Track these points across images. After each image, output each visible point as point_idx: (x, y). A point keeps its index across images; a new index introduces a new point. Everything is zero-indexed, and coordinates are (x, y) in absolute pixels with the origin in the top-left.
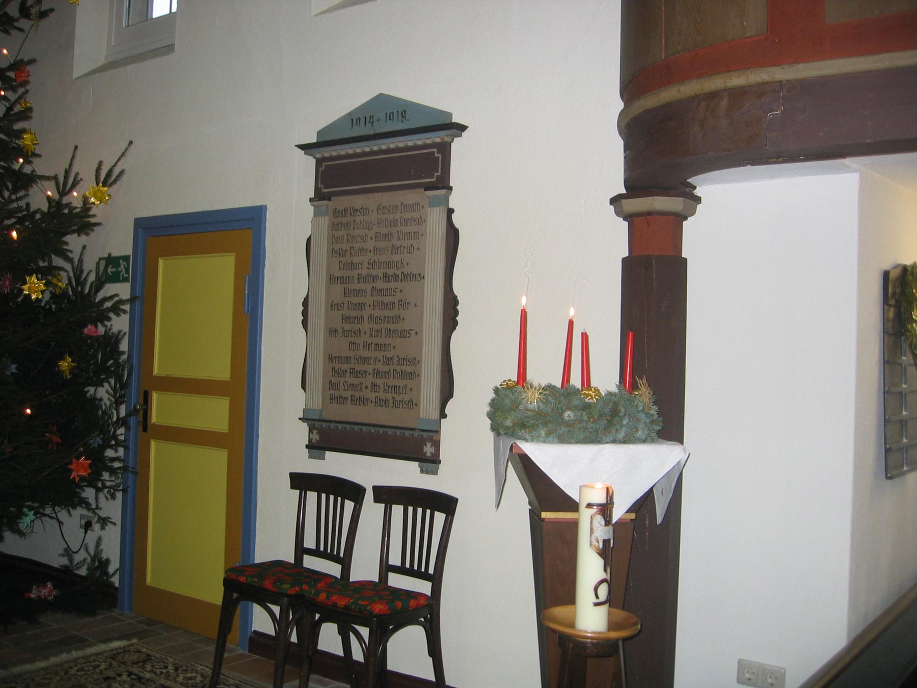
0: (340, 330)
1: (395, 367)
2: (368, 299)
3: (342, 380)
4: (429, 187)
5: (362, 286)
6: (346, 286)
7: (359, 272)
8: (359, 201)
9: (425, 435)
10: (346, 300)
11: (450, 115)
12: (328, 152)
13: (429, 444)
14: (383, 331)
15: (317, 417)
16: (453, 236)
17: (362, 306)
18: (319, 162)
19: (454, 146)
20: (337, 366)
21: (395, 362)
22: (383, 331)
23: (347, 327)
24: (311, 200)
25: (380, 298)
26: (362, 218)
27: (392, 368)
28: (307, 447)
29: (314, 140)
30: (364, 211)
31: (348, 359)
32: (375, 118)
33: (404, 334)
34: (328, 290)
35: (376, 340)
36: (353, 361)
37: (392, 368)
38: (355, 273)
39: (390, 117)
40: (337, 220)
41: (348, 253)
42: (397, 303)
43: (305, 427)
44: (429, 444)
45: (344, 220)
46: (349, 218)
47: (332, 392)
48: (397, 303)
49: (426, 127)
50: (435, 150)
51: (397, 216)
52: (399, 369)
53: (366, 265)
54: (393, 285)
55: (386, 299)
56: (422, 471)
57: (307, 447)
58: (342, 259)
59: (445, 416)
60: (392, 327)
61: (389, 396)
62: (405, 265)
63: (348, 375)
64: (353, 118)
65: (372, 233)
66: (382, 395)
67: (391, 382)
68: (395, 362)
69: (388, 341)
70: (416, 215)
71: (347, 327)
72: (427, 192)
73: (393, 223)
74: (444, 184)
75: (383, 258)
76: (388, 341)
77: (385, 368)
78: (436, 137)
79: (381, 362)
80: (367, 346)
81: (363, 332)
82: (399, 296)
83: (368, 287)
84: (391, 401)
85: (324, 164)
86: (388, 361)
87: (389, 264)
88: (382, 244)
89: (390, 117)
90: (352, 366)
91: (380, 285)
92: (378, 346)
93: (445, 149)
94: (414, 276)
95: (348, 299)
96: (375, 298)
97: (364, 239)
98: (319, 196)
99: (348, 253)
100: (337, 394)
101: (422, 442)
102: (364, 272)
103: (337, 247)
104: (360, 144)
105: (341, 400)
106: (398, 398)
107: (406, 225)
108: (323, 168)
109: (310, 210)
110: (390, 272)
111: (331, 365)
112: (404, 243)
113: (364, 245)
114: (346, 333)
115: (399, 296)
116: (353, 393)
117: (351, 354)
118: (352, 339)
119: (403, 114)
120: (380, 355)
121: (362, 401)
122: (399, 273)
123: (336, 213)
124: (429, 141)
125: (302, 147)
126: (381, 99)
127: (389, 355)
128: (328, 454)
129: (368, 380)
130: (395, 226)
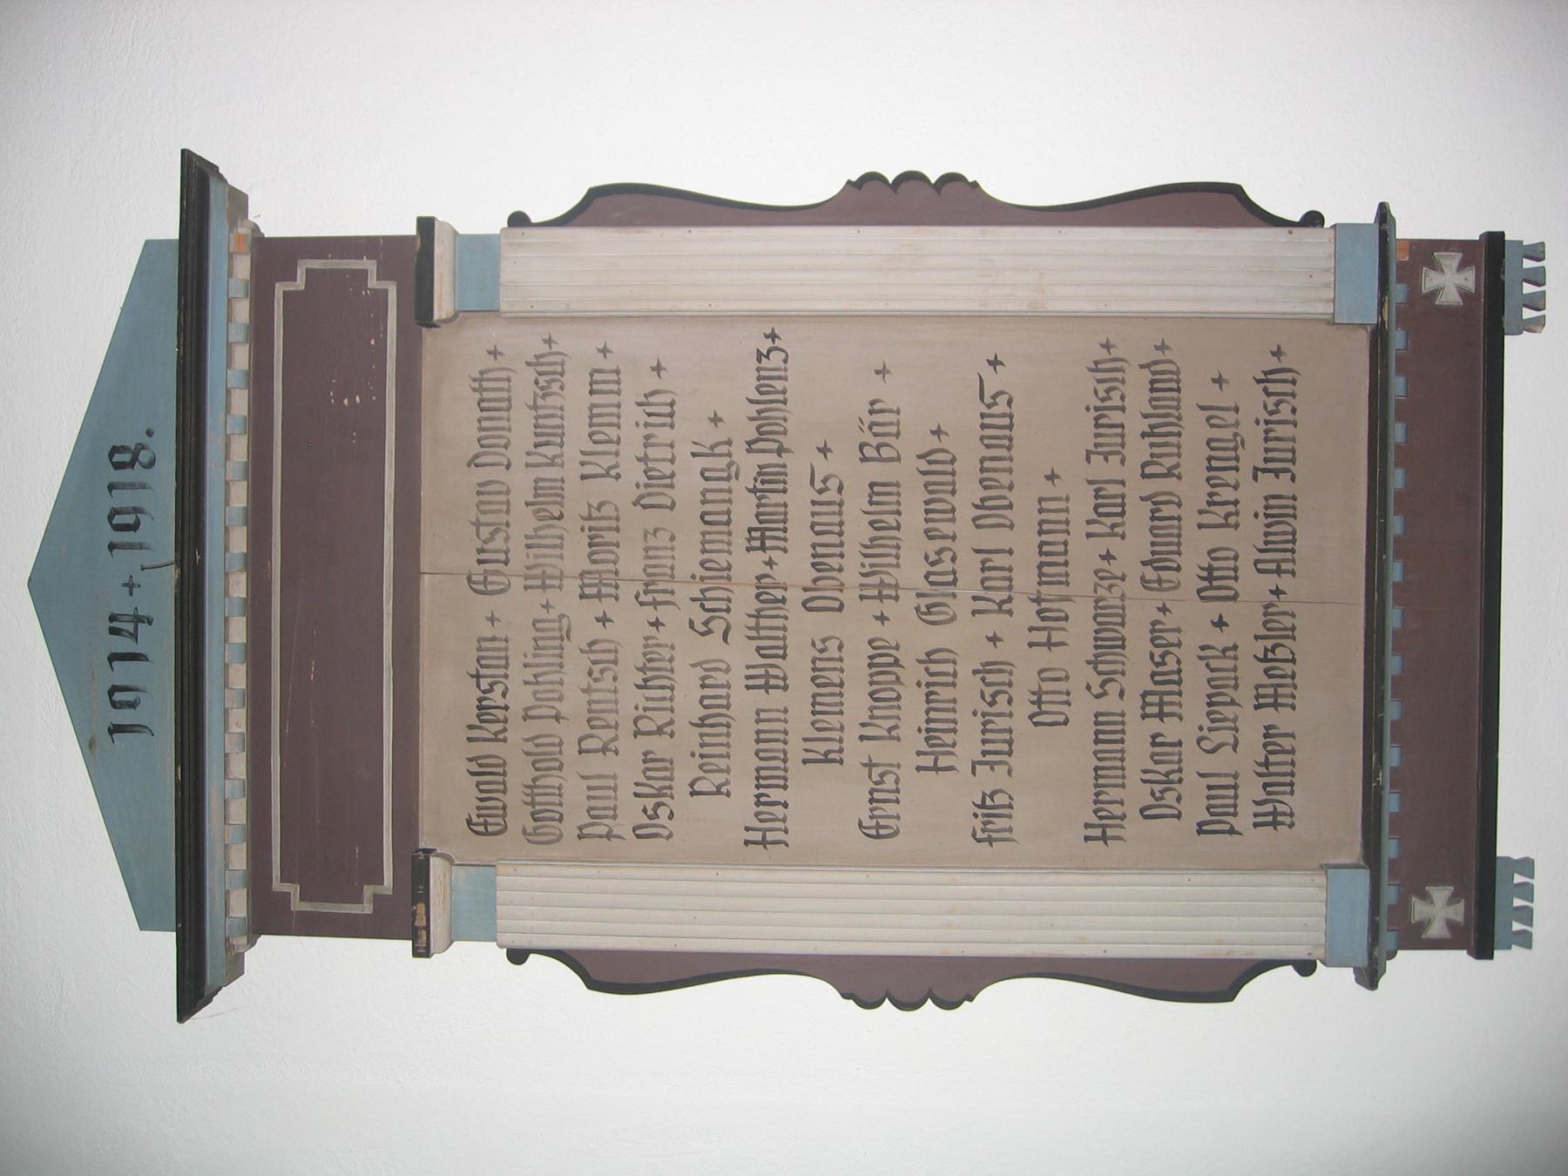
0: (988, 779)
1: (1131, 472)
2: (855, 629)
3: (1194, 761)
4: (420, 310)
5: (797, 666)
6: (796, 750)
7: (737, 678)
8: (445, 693)
9: (1398, 292)
10: (855, 751)
12: (228, 899)
13: (1430, 281)
14: (989, 539)
15: (1363, 877)
16: (609, 205)
17: (883, 661)
18: (269, 918)
20: (1136, 794)
21: (1112, 469)
22: (989, 539)
23: (968, 744)
24: (422, 951)
25: (852, 567)
26: (517, 674)
27: (1136, 488)
29: (166, 942)
30: (487, 668)
31: (1106, 732)
32: (124, 606)
33: (998, 430)
34: (813, 858)
35: (1025, 579)
36: (1111, 703)
37: (1136, 488)
38: (745, 703)
39: (125, 523)
40: (519, 818)
41: (659, 745)
42: (876, 471)
43: (1405, 966)
44: (1430, 281)
45: (519, 774)
46: (513, 752)
47: (1244, 821)
48: (876, 471)
49: (182, 329)
50: (297, 905)
51: (521, 482)
52: (1138, 450)
53: (712, 647)
54: (799, 499)
55: (857, 530)
56: (1537, 325)
57: (1483, 950)
58: (684, 774)
59: (1313, 219)
60: (968, 492)
61: (1251, 495)
62: (719, 434)
63: (1170, 729)
64: (105, 724)
65: (581, 616)
66: (1246, 539)
67: (1192, 488)
68: (1112, 469)
69: (1025, 513)
70: (523, 387)
71: (968, 744)
72: (443, 306)
73: (546, 501)
74: (413, 256)
75: (687, 560)
76: (1025, 513)
77: (1138, 517)
78: (231, 276)
79: (1113, 544)
80: (1049, 617)
81: (991, 653)
82: (843, 464)
83: (803, 628)
84: (1269, 484)
85: (278, 885)
86: (1108, 507)
87: (713, 521)
88: (631, 562)
89: (125, 523)
90: (1132, 705)
91: (794, 566)
92: (1051, 563)
93: (275, 256)
94: (764, 383)
95: (851, 736)
96: (850, 597)
97: (602, 659)
98: (405, 919)
99: (659, 745)
100: (1251, 789)
101: (1422, 309)
102: (740, 655)
103: (631, 812)
105: (1277, 769)
106: (1252, 455)
107: (560, 433)
108: (294, 890)
109: (471, 963)
110: (744, 511)
111: (1134, 826)
112: (632, 443)
113: (632, 656)
114: (997, 751)
115: (843, 464)
116: (1245, 695)
117: (1083, 709)
118: (1023, 708)
119: (124, 457)
120: (1083, 555)
121: (1276, 635)
122: (749, 465)
123: (485, 824)
124: (243, 311)
125: (193, 992)
126: (49, 586)
127: (1081, 508)
128: (1507, 846)
129: (1192, 619)
130: (501, 769)
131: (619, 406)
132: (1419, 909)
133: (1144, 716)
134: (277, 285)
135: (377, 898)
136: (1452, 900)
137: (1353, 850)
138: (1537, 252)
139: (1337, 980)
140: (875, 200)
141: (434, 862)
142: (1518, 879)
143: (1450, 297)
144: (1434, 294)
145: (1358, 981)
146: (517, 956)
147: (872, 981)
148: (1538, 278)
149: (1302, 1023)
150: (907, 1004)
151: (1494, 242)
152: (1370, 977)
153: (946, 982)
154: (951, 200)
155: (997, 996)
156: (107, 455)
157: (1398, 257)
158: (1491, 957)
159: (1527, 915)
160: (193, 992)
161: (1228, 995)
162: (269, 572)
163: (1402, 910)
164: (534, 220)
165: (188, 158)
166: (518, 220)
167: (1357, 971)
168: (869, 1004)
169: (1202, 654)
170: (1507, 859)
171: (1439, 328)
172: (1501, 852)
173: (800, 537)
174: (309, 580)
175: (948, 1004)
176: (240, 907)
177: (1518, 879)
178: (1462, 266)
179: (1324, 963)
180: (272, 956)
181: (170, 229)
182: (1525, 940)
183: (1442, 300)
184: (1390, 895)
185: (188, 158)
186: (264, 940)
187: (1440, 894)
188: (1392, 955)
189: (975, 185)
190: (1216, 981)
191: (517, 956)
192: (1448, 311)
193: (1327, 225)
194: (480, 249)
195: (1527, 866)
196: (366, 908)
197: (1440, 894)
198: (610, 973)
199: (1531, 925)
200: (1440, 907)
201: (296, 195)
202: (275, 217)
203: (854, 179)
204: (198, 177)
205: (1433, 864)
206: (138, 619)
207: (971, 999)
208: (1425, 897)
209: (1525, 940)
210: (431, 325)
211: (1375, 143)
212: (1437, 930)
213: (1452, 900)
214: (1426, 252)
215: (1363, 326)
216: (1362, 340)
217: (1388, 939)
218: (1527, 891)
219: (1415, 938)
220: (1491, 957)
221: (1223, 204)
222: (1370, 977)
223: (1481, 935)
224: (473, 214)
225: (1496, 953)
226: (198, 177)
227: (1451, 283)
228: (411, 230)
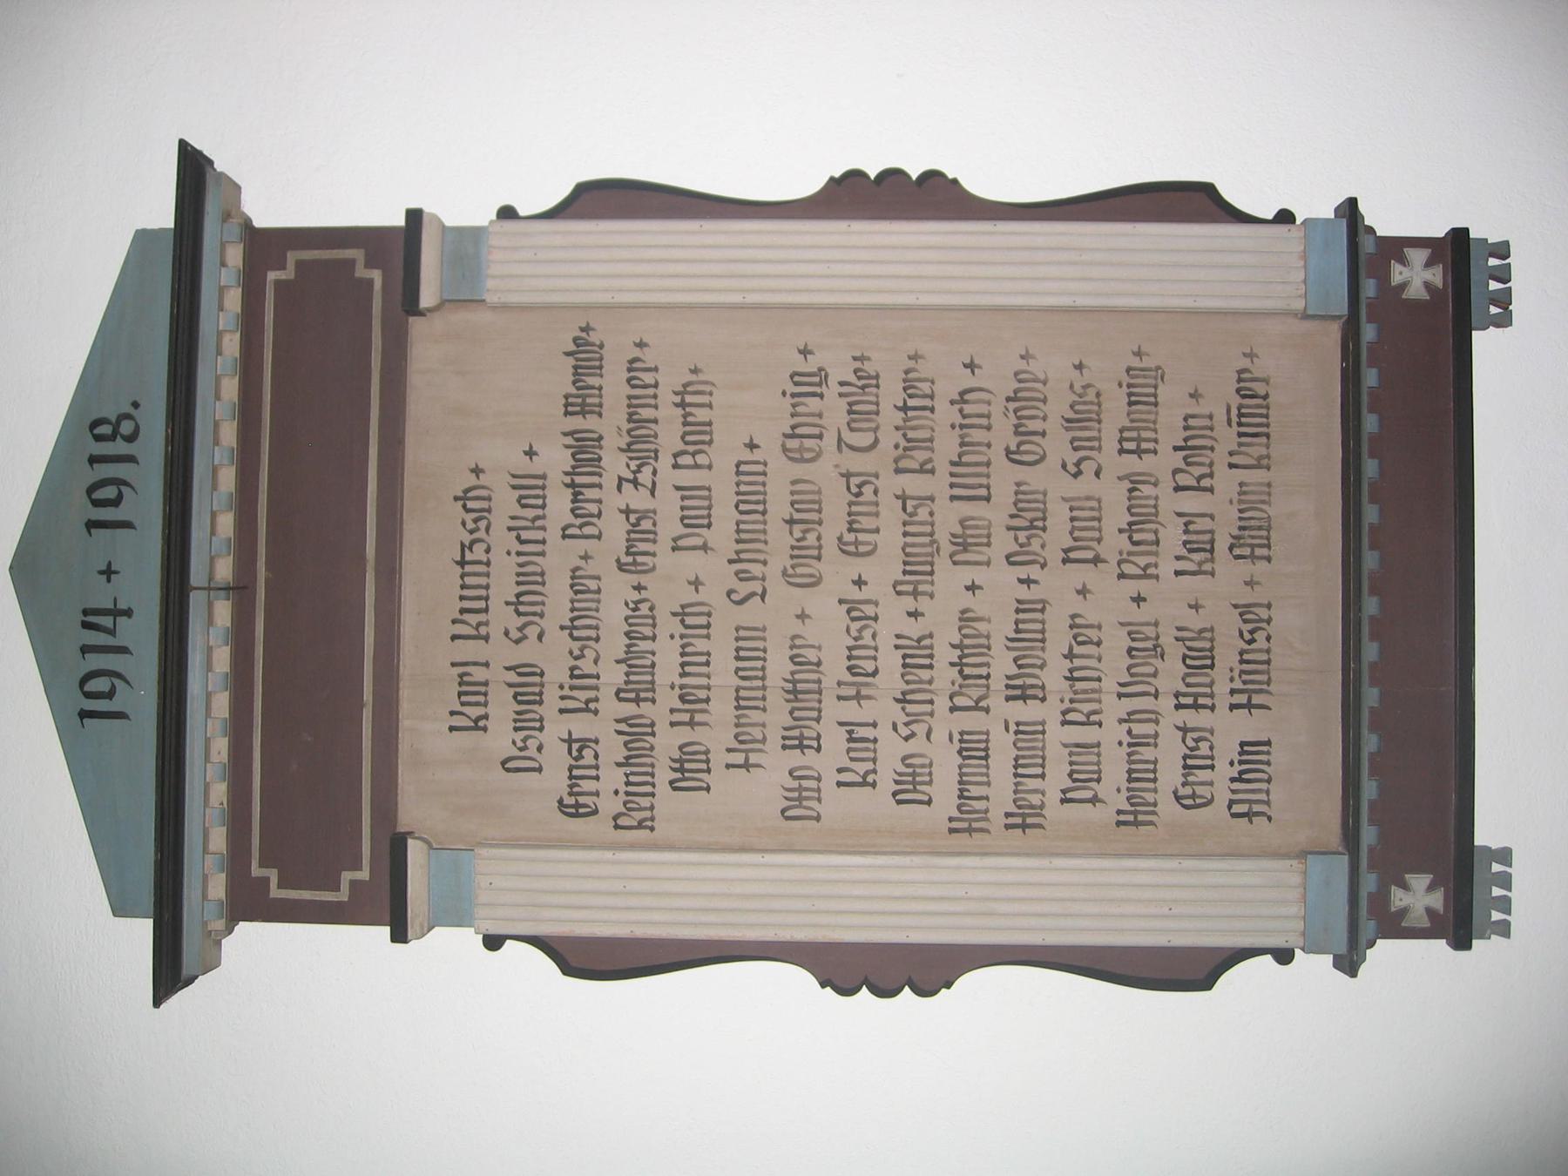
9: (1369, 288)
11: (143, 238)
12: (206, 883)
15: (1344, 861)
16: (600, 199)
18: (248, 904)
19: (263, 219)
24: (400, 935)
28: (1462, 941)
29: (142, 930)
43: (1385, 954)
44: (1398, 274)
50: (275, 892)
57: (1462, 941)
59: (1285, 217)
64: (84, 704)
72: (427, 299)
93: (266, 246)
104: (195, 659)
109: (448, 948)
125: (170, 975)
128: (1485, 834)
131: (487, 587)
132: (1399, 899)
133: (1122, 451)
134: (289, 254)
135: (354, 884)
136: (1431, 888)
137: (1332, 831)
138: (1502, 250)
139: (1315, 967)
140: (856, 196)
141: (411, 844)
142: (1496, 867)
143: (1416, 291)
144: (1403, 286)
145: (1335, 966)
146: (493, 942)
147: (850, 969)
148: (1503, 275)
149: (1279, 1005)
150: (885, 991)
151: (1459, 237)
152: (1349, 964)
153: (924, 969)
154: (932, 196)
155: (975, 983)
156: (95, 432)
157: (1367, 246)
158: (1469, 947)
159: (1505, 905)
160: (170, 975)
161: (1207, 983)
162: (382, 407)
163: (1380, 901)
164: (522, 213)
165: (183, 146)
166: (507, 213)
167: (1335, 957)
168: (846, 991)
169: (1180, 634)
170: (1487, 849)
171: (1410, 321)
172: (1480, 840)
173: (721, 709)
174: (294, 568)
175: (924, 991)
176: (218, 888)
177: (1496, 867)
178: (1429, 264)
179: (1303, 949)
180: (252, 943)
181: (163, 216)
182: (1504, 929)
183: (1396, 268)
184: (1369, 882)
185: (183, 146)
186: (243, 928)
187: (1419, 882)
188: (1371, 944)
189: (955, 181)
190: (1193, 970)
191: (493, 942)
192: (1416, 304)
193: (1298, 222)
194: (466, 242)
195: (1505, 856)
196: (343, 895)
197: (1419, 882)
198: (585, 959)
199: (1509, 914)
200: (1419, 895)
201: (281, 193)
202: (267, 208)
203: (837, 175)
204: (194, 169)
205: (1411, 852)
206: (116, 613)
207: (948, 985)
208: (1405, 886)
209: (1504, 929)
210: (421, 314)
211: (1344, 135)
212: (1418, 918)
213: (1431, 888)
214: (1396, 248)
215: (1339, 317)
216: (1334, 331)
217: (1368, 927)
218: (1506, 881)
219: (1395, 927)
220: (1469, 947)
221: (1196, 202)
222: (1349, 964)
223: (1459, 927)
224: (460, 205)
225: (1474, 942)
226: (194, 169)
227: (1417, 277)
228: (400, 221)
